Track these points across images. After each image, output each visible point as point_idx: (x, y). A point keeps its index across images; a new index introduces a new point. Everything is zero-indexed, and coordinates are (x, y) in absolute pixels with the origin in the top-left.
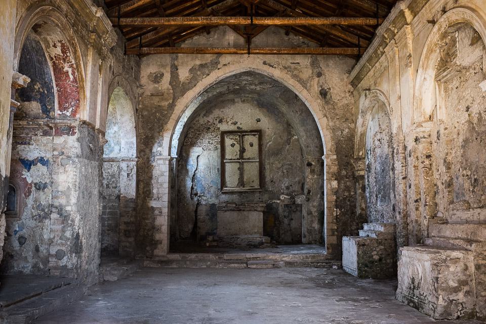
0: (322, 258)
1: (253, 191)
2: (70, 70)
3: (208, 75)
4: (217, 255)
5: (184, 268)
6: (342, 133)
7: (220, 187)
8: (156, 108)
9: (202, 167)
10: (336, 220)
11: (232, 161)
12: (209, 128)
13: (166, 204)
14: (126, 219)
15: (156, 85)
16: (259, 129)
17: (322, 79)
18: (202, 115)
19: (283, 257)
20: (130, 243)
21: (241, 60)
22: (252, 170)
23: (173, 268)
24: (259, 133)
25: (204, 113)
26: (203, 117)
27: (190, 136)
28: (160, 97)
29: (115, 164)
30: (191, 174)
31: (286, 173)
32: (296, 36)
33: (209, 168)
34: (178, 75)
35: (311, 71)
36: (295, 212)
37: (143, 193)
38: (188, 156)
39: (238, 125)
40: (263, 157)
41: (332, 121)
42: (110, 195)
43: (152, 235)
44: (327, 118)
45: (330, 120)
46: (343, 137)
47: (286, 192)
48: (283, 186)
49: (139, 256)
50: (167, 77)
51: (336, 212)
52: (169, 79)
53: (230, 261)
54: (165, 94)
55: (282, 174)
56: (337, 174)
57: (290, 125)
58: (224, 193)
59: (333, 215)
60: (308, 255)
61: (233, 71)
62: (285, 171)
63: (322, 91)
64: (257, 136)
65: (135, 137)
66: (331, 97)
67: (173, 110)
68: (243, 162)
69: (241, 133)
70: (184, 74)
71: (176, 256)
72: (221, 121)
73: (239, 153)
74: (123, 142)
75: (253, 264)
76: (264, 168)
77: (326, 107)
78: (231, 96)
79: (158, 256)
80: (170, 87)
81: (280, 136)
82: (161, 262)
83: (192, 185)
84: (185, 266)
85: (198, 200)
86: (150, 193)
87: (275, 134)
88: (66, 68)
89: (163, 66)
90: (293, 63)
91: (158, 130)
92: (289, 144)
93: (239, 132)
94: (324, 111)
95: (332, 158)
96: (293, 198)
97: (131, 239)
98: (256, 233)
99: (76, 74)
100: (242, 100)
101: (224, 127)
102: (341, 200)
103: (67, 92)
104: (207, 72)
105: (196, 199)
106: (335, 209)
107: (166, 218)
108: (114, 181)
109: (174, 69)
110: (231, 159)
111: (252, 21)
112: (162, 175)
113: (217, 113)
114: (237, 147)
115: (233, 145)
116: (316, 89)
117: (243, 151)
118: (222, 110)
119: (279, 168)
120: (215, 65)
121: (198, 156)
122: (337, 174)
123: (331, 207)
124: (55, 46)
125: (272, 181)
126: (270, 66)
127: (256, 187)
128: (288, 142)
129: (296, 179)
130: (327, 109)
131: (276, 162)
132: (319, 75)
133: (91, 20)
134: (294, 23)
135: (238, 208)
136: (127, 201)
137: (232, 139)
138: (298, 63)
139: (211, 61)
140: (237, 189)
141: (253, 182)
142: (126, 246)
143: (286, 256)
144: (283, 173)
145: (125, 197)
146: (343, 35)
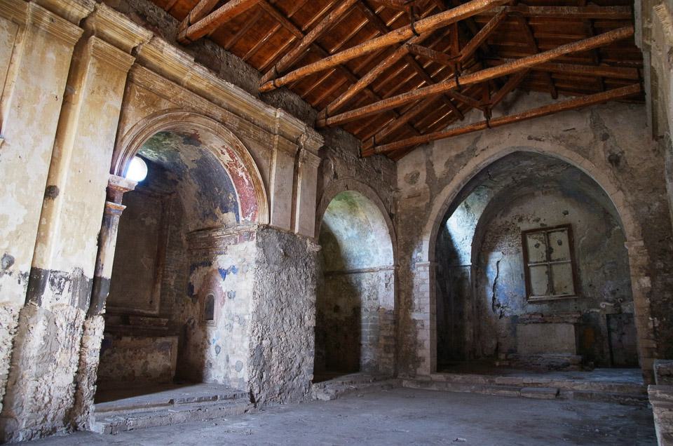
0: (636, 391)
1: (566, 299)
2: (243, 174)
3: (466, 164)
4: (488, 378)
5: (445, 391)
6: (649, 208)
7: (525, 296)
8: (413, 210)
9: (503, 274)
10: (655, 335)
11: (537, 264)
12: (508, 229)
13: (428, 316)
14: (385, 333)
15: (413, 186)
16: (566, 223)
17: (610, 142)
18: (499, 216)
19: (574, 385)
20: (390, 359)
21: (502, 141)
22: (563, 275)
23: (433, 391)
24: (568, 228)
25: (501, 212)
26: (500, 218)
27: (488, 240)
28: (418, 198)
29: (375, 274)
30: (491, 282)
31: (609, 274)
32: (567, 96)
33: (510, 274)
34: (434, 171)
35: (593, 135)
36: (627, 324)
37: (405, 304)
38: (487, 262)
39: (542, 221)
40: (576, 256)
41: (631, 194)
42: (371, 308)
43: (414, 352)
44: (623, 191)
45: (629, 194)
46: (651, 214)
47: (611, 298)
48: (607, 291)
49: (402, 374)
50: (423, 175)
51: (653, 322)
52: (425, 178)
53: (502, 386)
54: (422, 194)
55: (604, 276)
56: (648, 268)
57: (608, 213)
58: (531, 303)
59: (647, 327)
60: (613, 384)
61: (493, 155)
62: (607, 271)
63: (612, 158)
64: (566, 232)
65: (391, 244)
66: (626, 162)
67: (431, 210)
68: (551, 264)
69: (546, 231)
70: (439, 169)
71: (440, 377)
72: (521, 220)
73: (545, 254)
74: (380, 250)
75: (528, 392)
76: (579, 269)
77: (620, 177)
78: (525, 189)
79: (421, 376)
80: (426, 185)
81: (597, 229)
82: (421, 382)
83: (494, 295)
84: (446, 389)
85: (501, 311)
86: (411, 304)
87: (588, 227)
88: (241, 174)
89: (418, 164)
90: (567, 130)
91: (417, 234)
92: (609, 238)
93: (543, 229)
94: (618, 183)
95: (636, 245)
96: (617, 305)
97: (391, 356)
98: (566, 351)
99: (249, 177)
100: (544, 191)
101: (525, 226)
102: (660, 305)
103: (246, 197)
104: (464, 161)
105: (498, 311)
106: (650, 319)
107: (429, 331)
108: (374, 293)
109: (430, 165)
110: (537, 262)
111: (457, 82)
112: (423, 283)
113: (515, 211)
114: (543, 248)
115: (537, 246)
116: (603, 155)
117: (550, 251)
118: (520, 207)
119: (598, 269)
120: (472, 152)
121: (498, 262)
122: (648, 268)
123: (643, 316)
124: (223, 153)
125: (591, 285)
126: (537, 139)
127: (571, 294)
128: (608, 234)
129: (625, 281)
130: (621, 180)
131: (595, 261)
132: (605, 137)
133: (274, 123)
134: (510, 69)
135: (544, 320)
136: (386, 313)
137: (535, 238)
138: (574, 129)
139: (468, 148)
140: (545, 298)
141: (566, 287)
142: (385, 363)
143: (579, 384)
144: (605, 273)
145: (384, 309)
146: (612, 74)
